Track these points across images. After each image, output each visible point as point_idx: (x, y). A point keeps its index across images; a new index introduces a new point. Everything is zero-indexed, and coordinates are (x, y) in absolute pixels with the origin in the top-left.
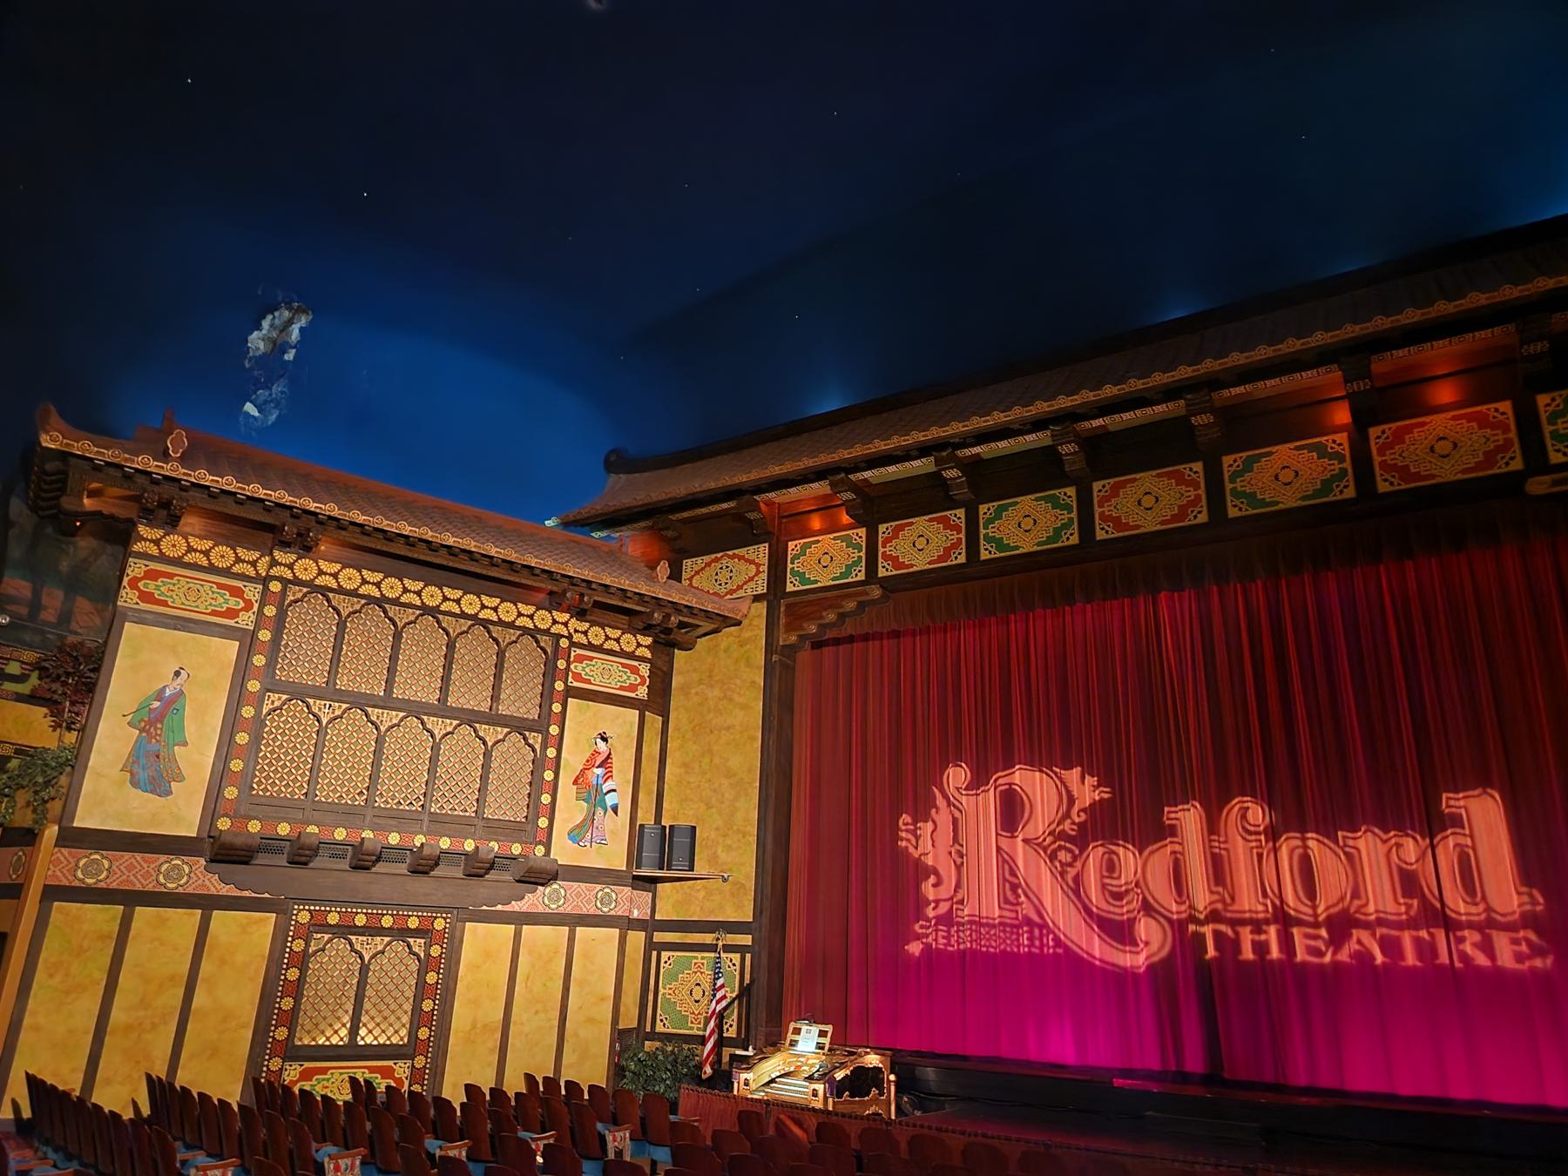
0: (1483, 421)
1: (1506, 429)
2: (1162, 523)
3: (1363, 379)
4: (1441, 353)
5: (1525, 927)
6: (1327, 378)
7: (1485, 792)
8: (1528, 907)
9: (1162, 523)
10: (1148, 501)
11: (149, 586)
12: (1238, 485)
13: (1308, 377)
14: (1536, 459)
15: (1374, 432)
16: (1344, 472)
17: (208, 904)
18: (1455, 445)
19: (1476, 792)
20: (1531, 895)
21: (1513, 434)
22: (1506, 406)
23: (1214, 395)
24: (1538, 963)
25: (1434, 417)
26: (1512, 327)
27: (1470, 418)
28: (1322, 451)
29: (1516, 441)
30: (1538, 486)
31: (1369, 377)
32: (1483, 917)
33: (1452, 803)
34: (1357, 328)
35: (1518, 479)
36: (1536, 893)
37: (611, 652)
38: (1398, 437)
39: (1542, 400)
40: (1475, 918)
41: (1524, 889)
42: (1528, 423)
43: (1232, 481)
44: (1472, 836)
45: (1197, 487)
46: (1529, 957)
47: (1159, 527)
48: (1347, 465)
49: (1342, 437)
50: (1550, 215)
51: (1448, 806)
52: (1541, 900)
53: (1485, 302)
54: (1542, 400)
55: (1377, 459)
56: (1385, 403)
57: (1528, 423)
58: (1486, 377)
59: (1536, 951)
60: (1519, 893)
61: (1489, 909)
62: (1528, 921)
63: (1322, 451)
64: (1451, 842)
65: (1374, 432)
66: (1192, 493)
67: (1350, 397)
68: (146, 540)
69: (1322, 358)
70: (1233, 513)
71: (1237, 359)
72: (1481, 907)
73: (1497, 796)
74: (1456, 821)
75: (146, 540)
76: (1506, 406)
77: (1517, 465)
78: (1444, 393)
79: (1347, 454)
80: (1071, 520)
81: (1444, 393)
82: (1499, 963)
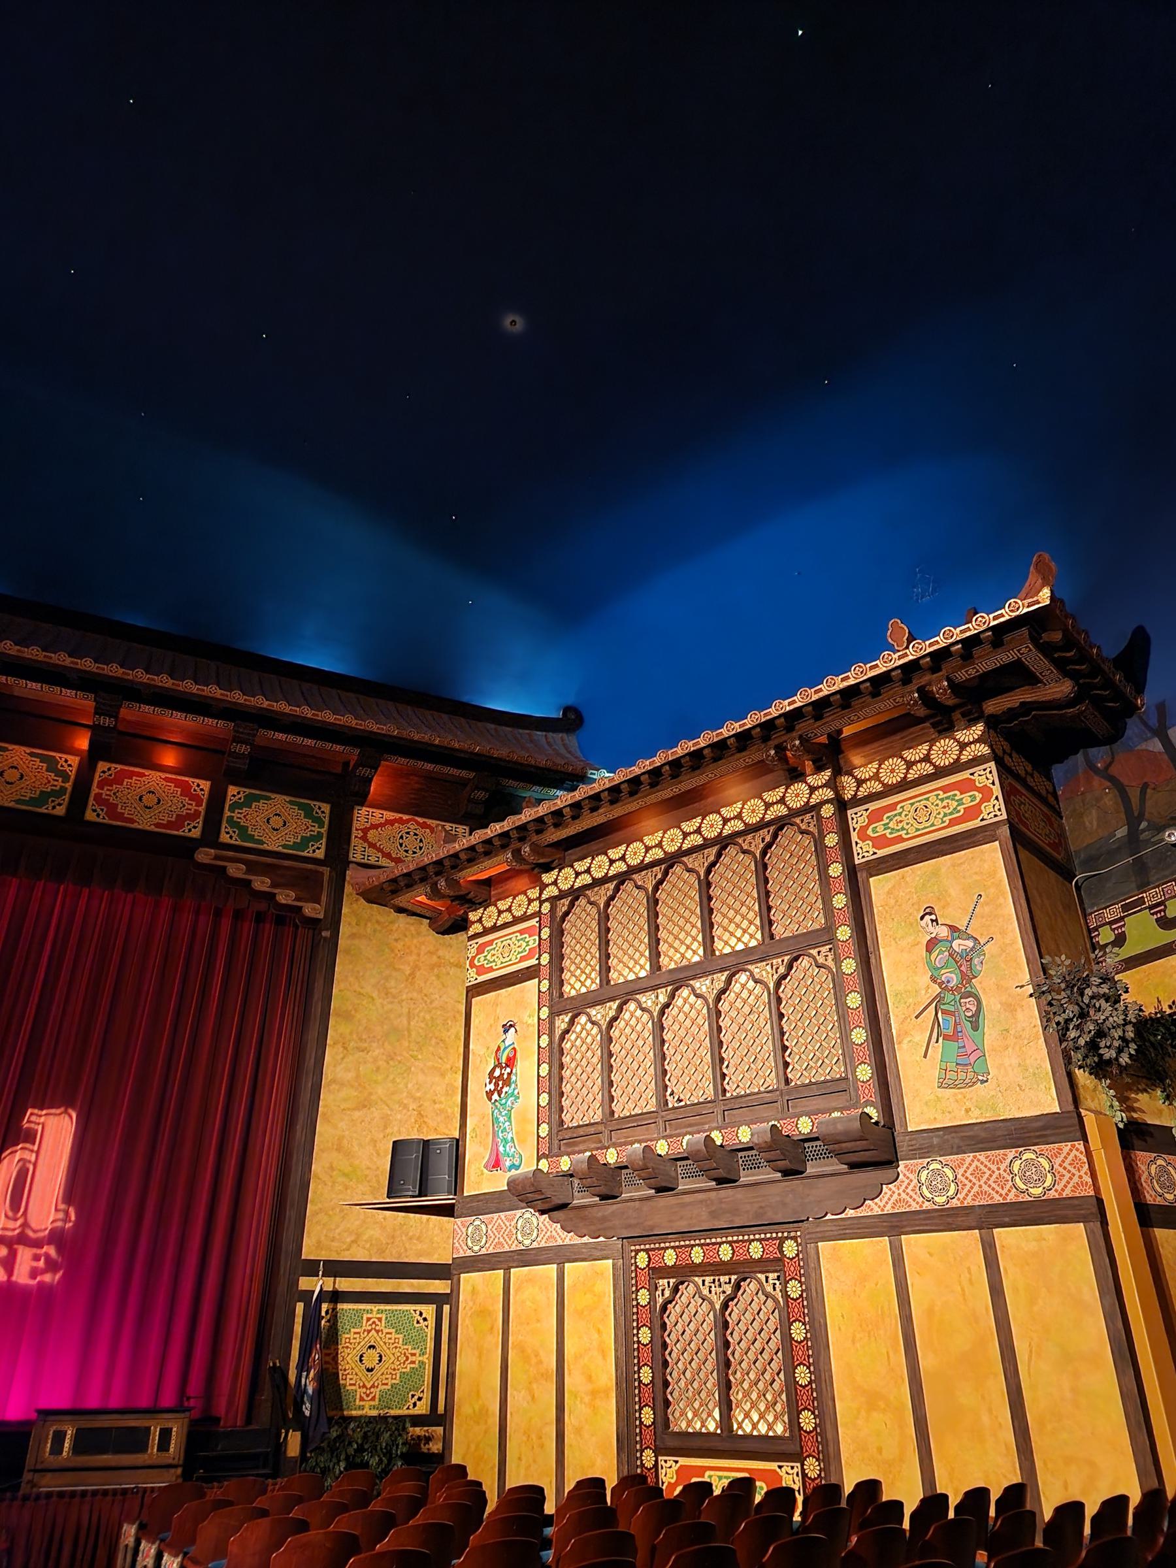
0: (186, 790)
1: (199, 804)
2: (157, 825)
3: (110, 717)
4: (178, 722)
5: (49, 1244)
6: (85, 702)
7: (66, 1112)
8: (59, 1224)
9: (284, 846)
10: (276, 822)
11: (967, 800)
12: (194, 808)
13: (68, 696)
14: (210, 836)
15: (102, 766)
16: (63, 790)
17: (560, 1256)
18: (22, 776)
19: (58, 1111)
20: (67, 1213)
21: (202, 809)
22: (206, 785)
23: (262, 731)
24: (47, 1278)
25: (153, 773)
26: (357, 751)
27: (178, 784)
28: (52, 765)
29: (325, 835)
30: (204, 856)
31: (116, 717)
32: (17, 1232)
33: (33, 1118)
34: (122, 670)
35: (190, 846)
36: (72, 1211)
37: (506, 925)
38: (119, 779)
39: (232, 790)
40: (10, 1233)
41: (62, 1206)
42: (216, 801)
43: (232, 809)
44: (38, 1153)
45: (199, 804)
46: (43, 1272)
47: (12, 804)
48: (69, 786)
49: (74, 761)
50: (118, 617)
51: (28, 1121)
52: (73, 1218)
53: (309, 716)
54: (232, 790)
55: (95, 790)
56: (121, 746)
57: (216, 801)
58: (204, 758)
59: (51, 1266)
60: (57, 1210)
61: (25, 1225)
62: (56, 1237)
63: (52, 765)
64: (17, 1156)
65: (102, 766)
66: (194, 808)
67: (95, 729)
68: (975, 742)
69: (84, 682)
70: (90, 816)
71: (165, 681)
72: (19, 1223)
73: (74, 1116)
74: (30, 1137)
75: (975, 742)
76: (206, 785)
77: (196, 833)
78: (170, 758)
79: (73, 776)
80: (63, 789)
81: (170, 758)
82: (14, 1278)
